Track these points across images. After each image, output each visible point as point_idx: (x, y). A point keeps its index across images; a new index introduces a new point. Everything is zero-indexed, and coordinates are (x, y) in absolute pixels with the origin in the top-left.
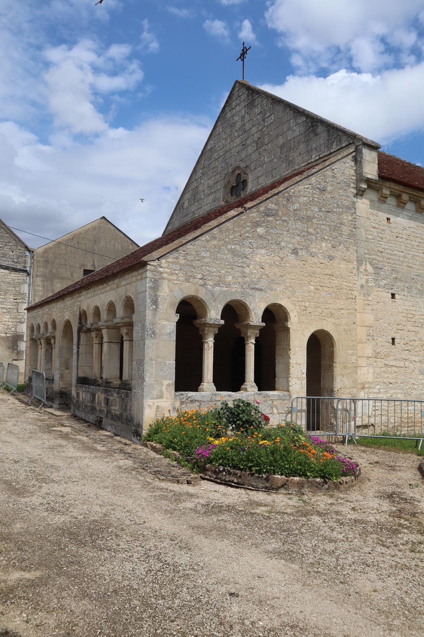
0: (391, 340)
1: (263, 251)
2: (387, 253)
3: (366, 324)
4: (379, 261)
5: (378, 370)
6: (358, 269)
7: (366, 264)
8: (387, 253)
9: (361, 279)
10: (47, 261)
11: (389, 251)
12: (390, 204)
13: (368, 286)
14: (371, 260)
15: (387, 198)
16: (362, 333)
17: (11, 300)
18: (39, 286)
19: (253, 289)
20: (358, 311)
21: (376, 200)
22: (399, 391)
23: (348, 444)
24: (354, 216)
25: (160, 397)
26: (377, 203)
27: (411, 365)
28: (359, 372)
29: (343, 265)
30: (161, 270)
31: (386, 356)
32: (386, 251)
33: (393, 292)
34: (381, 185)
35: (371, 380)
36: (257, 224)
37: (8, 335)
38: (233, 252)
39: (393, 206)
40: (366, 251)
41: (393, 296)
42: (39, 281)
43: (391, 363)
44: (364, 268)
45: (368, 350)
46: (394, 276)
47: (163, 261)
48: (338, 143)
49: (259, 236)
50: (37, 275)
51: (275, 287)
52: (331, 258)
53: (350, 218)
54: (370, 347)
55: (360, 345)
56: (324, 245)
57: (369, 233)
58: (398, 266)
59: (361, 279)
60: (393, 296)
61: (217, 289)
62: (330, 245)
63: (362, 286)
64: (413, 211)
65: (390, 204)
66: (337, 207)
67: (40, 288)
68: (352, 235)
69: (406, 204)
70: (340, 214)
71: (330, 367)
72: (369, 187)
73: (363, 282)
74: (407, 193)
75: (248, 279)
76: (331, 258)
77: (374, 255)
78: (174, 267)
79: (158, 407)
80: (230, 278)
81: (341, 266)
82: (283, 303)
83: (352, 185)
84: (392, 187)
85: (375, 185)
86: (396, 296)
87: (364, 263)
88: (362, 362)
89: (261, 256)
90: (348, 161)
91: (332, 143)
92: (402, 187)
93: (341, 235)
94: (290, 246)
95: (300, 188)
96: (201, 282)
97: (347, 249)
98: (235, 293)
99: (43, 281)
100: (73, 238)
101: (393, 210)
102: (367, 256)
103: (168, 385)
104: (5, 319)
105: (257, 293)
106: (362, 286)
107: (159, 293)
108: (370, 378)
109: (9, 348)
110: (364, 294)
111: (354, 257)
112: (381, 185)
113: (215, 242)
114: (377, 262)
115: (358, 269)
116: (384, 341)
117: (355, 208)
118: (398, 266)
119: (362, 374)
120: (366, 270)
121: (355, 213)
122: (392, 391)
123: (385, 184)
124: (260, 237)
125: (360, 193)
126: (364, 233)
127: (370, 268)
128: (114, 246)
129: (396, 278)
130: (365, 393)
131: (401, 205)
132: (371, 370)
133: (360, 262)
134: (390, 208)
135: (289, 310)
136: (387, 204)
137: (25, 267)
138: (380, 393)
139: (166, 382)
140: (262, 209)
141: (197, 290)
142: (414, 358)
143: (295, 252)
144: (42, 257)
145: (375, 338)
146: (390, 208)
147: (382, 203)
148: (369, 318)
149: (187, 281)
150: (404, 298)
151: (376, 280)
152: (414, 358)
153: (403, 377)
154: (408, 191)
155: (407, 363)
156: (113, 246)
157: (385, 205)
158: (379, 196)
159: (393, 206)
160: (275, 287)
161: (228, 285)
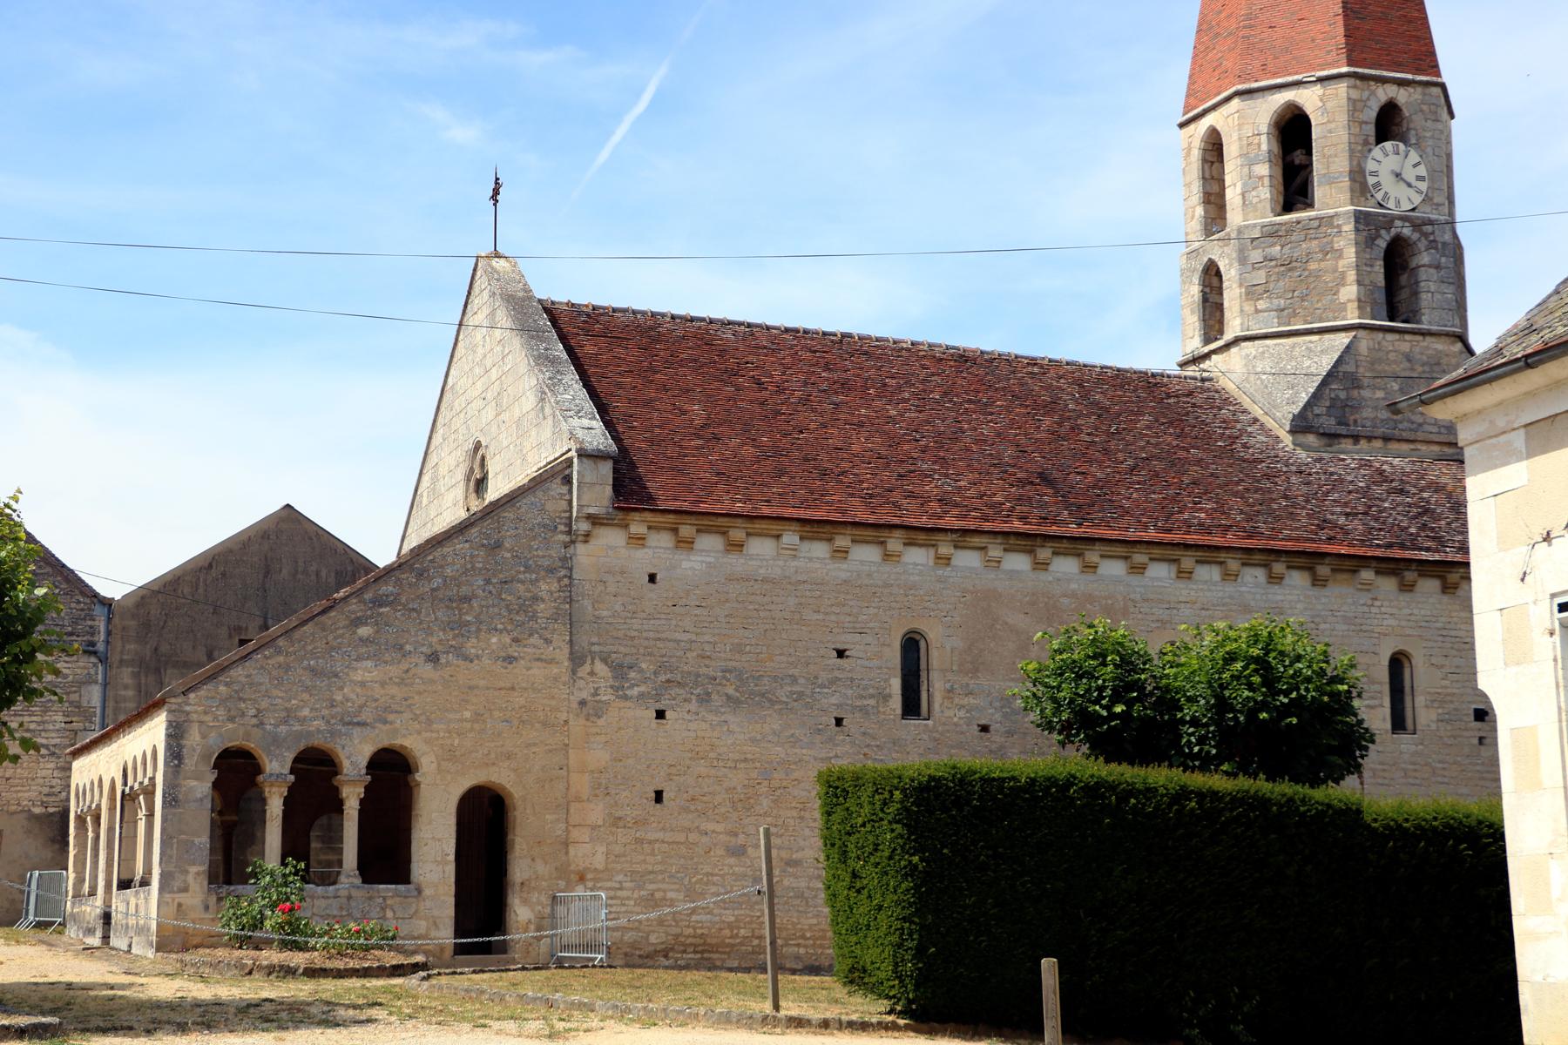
1: (369, 664)
10: (146, 626)
11: (651, 635)
17: (58, 726)
18: (126, 687)
19: (349, 723)
25: (185, 890)
26: (623, 551)
27: (705, 839)
29: (538, 671)
30: (188, 708)
33: (660, 707)
35: (600, 867)
36: (357, 622)
37: (51, 810)
38: (314, 672)
40: (595, 640)
41: (660, 715)
42: (126, 675)
45: (596, 813)
47: (192, 695)
49: (361, 639)
50: (121, 661)
51: (391, 717)
52: (510, 659)
56: (494, 640)
60: (660, 715)
61: (283, 729)
63: (583, 703)
67: (130, 693)
72: (594, 524)
75: (339, 709)
78: (209, 702)
79: (180, 905)
80: (306, 712)
81: (534, 671)
82: (407, 742)
83: (562, 528)
89: (365, 672)
93: (534, 617)
94: (424, 649)
95: (446, 550)
96: (254, 721)
97: (548, 641)
98: (314, 728)
99: (136, 675)
100: (210, 566)
102: (596, 648)
103: (198, 874)
104: (44, 773)
105: (356, 731)
107: (184, 742)
108: (599, 861)
109: (53, 841)
111: (563, 654)
113: (281, 659)
122: (652, 887)
124: (364, 641)
128: (318, 574)
133: (577, 660)
135: (418, 754)
137: (93, 644)
139: (193, 869)
140: (368, 596)
141: (247, 736)
142: (710, 826)
143: (433, 658)
144: (134, 616)
148: (599, 756)
149: (231, 719)
150: (687, 717)
152: (710, 826)
155: (693, 837)
156: (313, 577)
160: (391, 717)
161: (303, 721)
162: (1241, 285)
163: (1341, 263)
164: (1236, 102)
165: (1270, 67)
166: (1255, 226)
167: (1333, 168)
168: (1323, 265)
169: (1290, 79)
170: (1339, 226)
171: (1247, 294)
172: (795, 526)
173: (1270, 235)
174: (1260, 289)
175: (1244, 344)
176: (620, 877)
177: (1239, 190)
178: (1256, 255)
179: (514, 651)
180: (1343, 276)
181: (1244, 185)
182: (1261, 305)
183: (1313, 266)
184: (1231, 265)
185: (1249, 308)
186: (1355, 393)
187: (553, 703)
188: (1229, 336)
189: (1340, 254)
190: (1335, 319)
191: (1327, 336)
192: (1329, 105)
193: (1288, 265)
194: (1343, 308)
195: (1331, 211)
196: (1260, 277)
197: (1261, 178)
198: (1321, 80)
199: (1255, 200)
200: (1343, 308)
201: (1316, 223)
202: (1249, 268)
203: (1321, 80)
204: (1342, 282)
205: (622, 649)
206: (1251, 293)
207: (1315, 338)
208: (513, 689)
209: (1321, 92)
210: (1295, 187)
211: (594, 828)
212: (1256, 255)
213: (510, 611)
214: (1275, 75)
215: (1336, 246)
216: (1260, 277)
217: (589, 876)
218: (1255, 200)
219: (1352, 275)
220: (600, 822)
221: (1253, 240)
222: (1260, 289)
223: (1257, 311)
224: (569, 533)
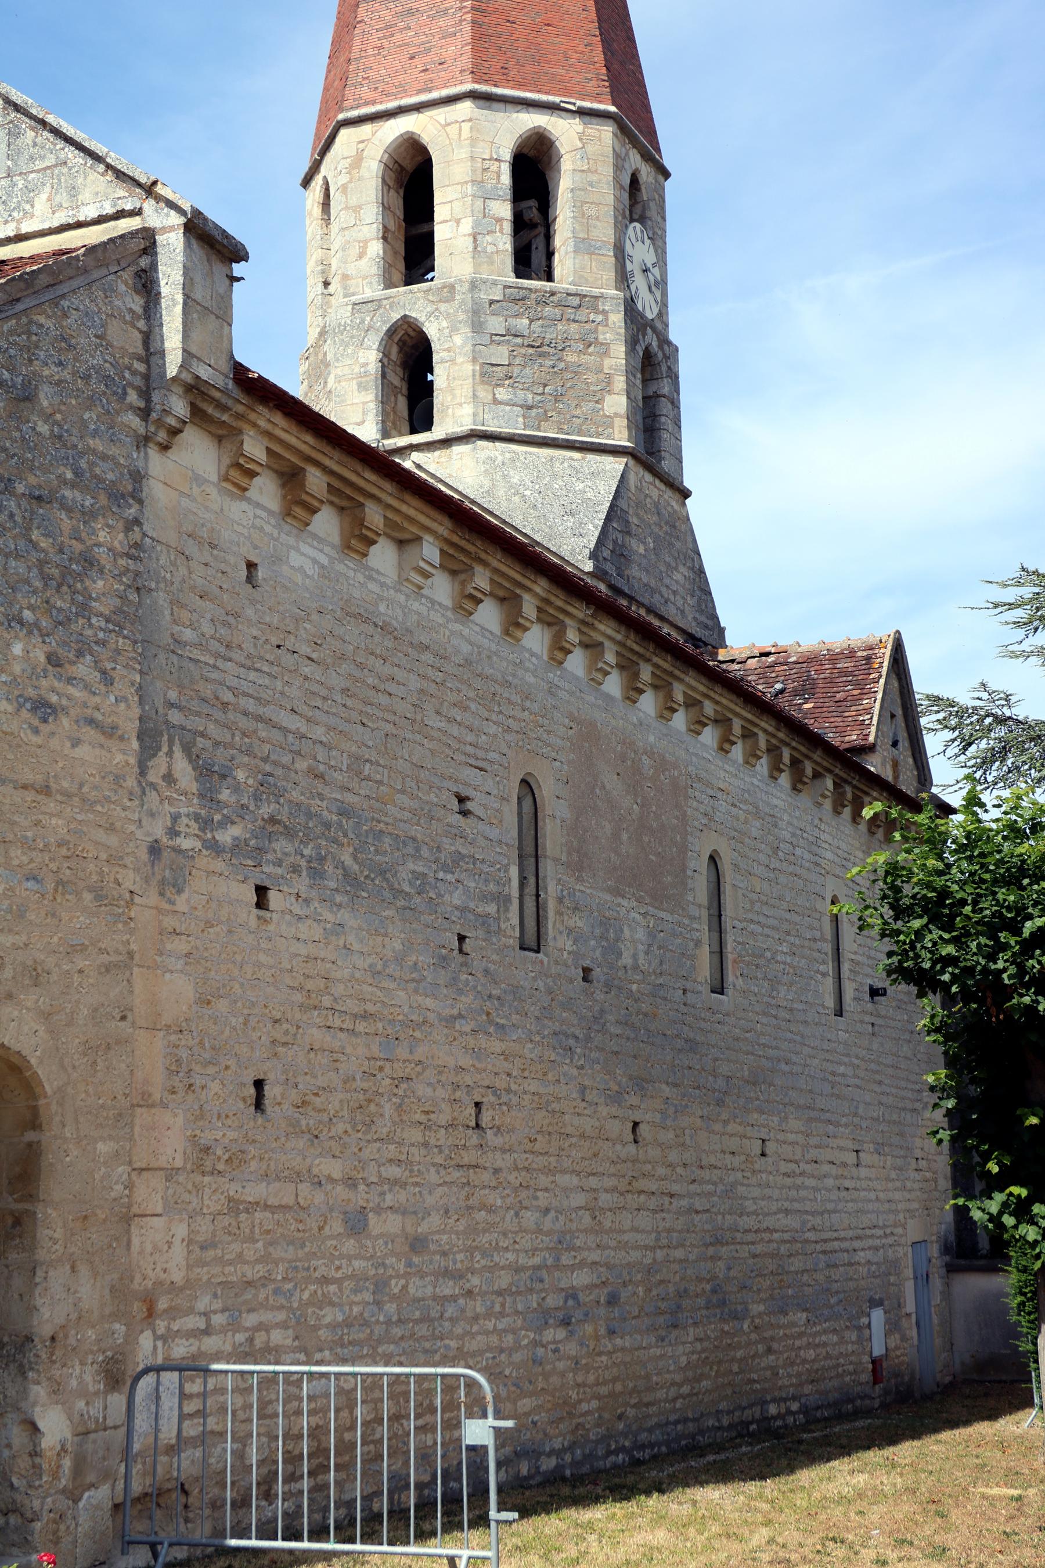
0: (252, 1091)
2: (245, 713)
3: (167, 1019)
4: (217, 744)
5: (204, 1227)
6: (143, 772)
7: (170, 754)
8: (245, 713)
9: (152, 815)
11: (251, 705)
12: (258, 505)
13: (178, 850)
14: (189, 737)
15: (252, 474)
16: (151, 1055)
20: (137, 957)
21: (214, 478)
22: (281, 1316)
23: (469, 1528)
24: (136, 535)
26: (214, 492)
27: (319, 1197)
28: (136, 1241)
31: (236, 1159)
32: (243, 701)
34: (239, 417)
35: (178, 1276)
39: (270, 513)
40: (173, 695)
43: (255, 1191)
44: (163, 770)
45: (169, 1138)
46: (265, 810)
48: (62, 197)
53: (119, 540)
54: (180, 1120)
55: (142, 1116)
57: (185, 615)
58: (279, 772)
59: (152, 815)
62: (40, 656)
63: (155, 849)
64: (333, 546)
65: (258, 505)
66: (73, 486)
68: (120, 619)
69: (314, 511)
70: (89, 515)
71: (17, 1222)
72: (198, 414)
73: (158, 830)
74: (325, 469)
76: (44, 709)
77: (198, 714)
81: (83, 752)
83: (133, 397)
84: (279, 432)
85: (217, 414)
86: (272, 895)
87: (165, 749)
88: (150, 1194)
90: (122, 288)
91: (31, 191)
92: (309, 438)
93: (84, 610)
97: (107, 679)
101: (268, 529)
102: (175, 717)
106: (155, 849)
108: (175, 1265)
110: (163, 882)
112: (239, 417)
114: (208, 744)
115: (143, 772)
116: (225, 1092)
117: (140, 502)
118: (279, 772)
119: (149, 1248)
120: (169, 778)
121: (137, 522)
123: (253, 416)
125: (162, 436)
126: (167, 612)
127: (182, 767)
129: (272, 820)
130: (156, 1338)
131: (298, 511)
132: (181, 1230)
133: (150, 738)
134: (258, 522)
136: (249, 500)
138: (207, 1332)
145: (198, 1081)
146: (258, 522)
147: (232, 496)
151: (205, 824)
153: (290, 1253)
154: (327, 462)
157: (244, 505)
158: (226, 461)
159: (270, 513)
162: (474, 360)
163: (607, 362)
164: (467, 105)
165: (513, 73)
166: (495, 283)
167: (594, 233)
168: (584, 359)
169: (544, 98)
170: (605, 313)
171: (483, 375)
172: (443, 526)
173: (515, 301)
174: (500, 372)
175: (480, 443)
176: (203, 1303)
177: (467, 226)
178: (496, 324)
179: (50, 688)
180: (609, 379)
181: (476, 224)
182: (502, 394)
183: (571, 357)
184: (454, 330)
185: (484, 394)
186: (627, 539)
187: (113, 841)
188: (438, 432)
189: (605, 350)
190: (599, 435)
191: (590, 457)
192: (590, 148)
193: (538, 348)
194: (608, 422)
195: (596, 292)
196: (500, 354)
197: (499, 220)
198: (582, 112)
199: (490, 249)
200: (608, 422)
201: (576, 301)
202: (486, 339)
203: (582, 112)
204: (607, 387)
205: (212, 729)
206: (489, 374)
207: (577, 455)
208: (46, 790)
209: (580, 128)
210: (532, 252)
211: (171, 1174)
212: (496, 324)
213: (46, 578)
214: (520, 86)
215: (601, 337)
216: (500, 354)
217: (162, 1304)
218: (490, 249)
219: (620, 382)
220: (179, 1163)
221: (492, 302)
222: (500, 372)
223: (495, 401)
224: (145, 413)
